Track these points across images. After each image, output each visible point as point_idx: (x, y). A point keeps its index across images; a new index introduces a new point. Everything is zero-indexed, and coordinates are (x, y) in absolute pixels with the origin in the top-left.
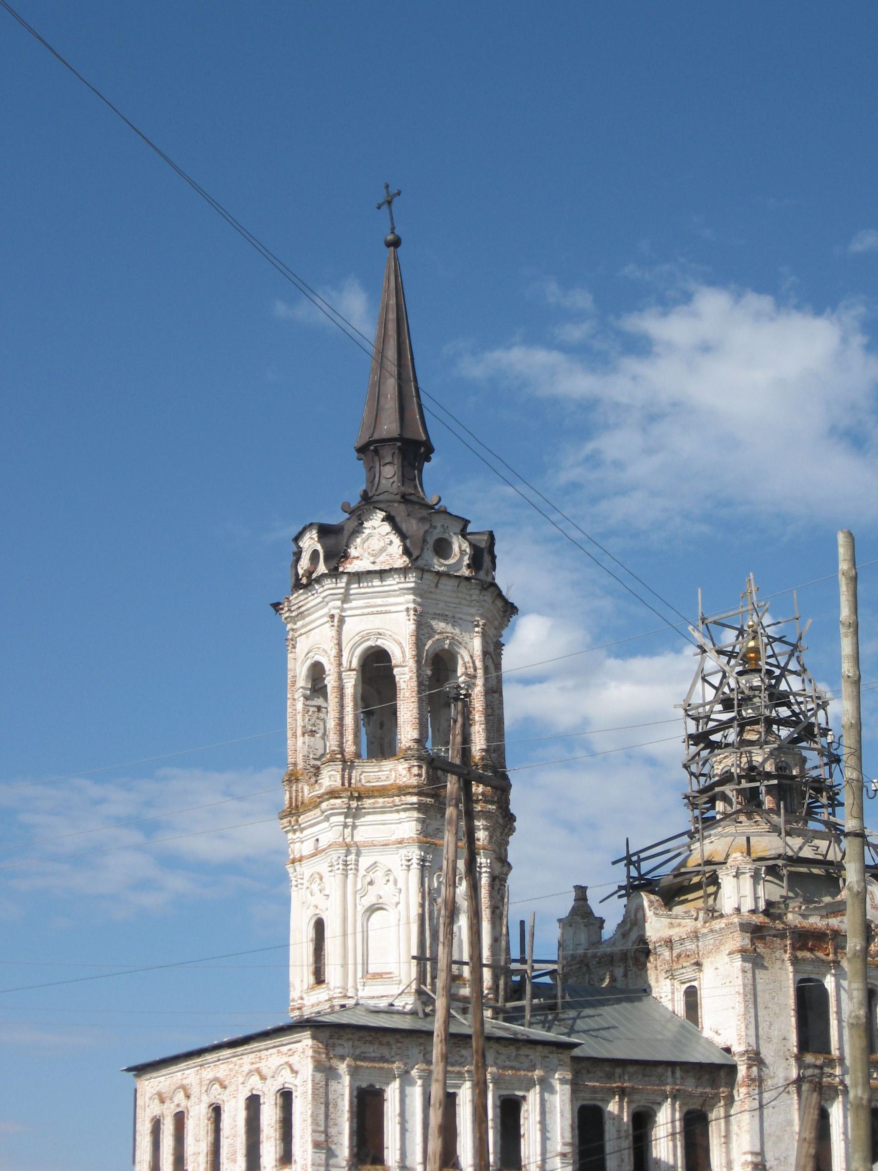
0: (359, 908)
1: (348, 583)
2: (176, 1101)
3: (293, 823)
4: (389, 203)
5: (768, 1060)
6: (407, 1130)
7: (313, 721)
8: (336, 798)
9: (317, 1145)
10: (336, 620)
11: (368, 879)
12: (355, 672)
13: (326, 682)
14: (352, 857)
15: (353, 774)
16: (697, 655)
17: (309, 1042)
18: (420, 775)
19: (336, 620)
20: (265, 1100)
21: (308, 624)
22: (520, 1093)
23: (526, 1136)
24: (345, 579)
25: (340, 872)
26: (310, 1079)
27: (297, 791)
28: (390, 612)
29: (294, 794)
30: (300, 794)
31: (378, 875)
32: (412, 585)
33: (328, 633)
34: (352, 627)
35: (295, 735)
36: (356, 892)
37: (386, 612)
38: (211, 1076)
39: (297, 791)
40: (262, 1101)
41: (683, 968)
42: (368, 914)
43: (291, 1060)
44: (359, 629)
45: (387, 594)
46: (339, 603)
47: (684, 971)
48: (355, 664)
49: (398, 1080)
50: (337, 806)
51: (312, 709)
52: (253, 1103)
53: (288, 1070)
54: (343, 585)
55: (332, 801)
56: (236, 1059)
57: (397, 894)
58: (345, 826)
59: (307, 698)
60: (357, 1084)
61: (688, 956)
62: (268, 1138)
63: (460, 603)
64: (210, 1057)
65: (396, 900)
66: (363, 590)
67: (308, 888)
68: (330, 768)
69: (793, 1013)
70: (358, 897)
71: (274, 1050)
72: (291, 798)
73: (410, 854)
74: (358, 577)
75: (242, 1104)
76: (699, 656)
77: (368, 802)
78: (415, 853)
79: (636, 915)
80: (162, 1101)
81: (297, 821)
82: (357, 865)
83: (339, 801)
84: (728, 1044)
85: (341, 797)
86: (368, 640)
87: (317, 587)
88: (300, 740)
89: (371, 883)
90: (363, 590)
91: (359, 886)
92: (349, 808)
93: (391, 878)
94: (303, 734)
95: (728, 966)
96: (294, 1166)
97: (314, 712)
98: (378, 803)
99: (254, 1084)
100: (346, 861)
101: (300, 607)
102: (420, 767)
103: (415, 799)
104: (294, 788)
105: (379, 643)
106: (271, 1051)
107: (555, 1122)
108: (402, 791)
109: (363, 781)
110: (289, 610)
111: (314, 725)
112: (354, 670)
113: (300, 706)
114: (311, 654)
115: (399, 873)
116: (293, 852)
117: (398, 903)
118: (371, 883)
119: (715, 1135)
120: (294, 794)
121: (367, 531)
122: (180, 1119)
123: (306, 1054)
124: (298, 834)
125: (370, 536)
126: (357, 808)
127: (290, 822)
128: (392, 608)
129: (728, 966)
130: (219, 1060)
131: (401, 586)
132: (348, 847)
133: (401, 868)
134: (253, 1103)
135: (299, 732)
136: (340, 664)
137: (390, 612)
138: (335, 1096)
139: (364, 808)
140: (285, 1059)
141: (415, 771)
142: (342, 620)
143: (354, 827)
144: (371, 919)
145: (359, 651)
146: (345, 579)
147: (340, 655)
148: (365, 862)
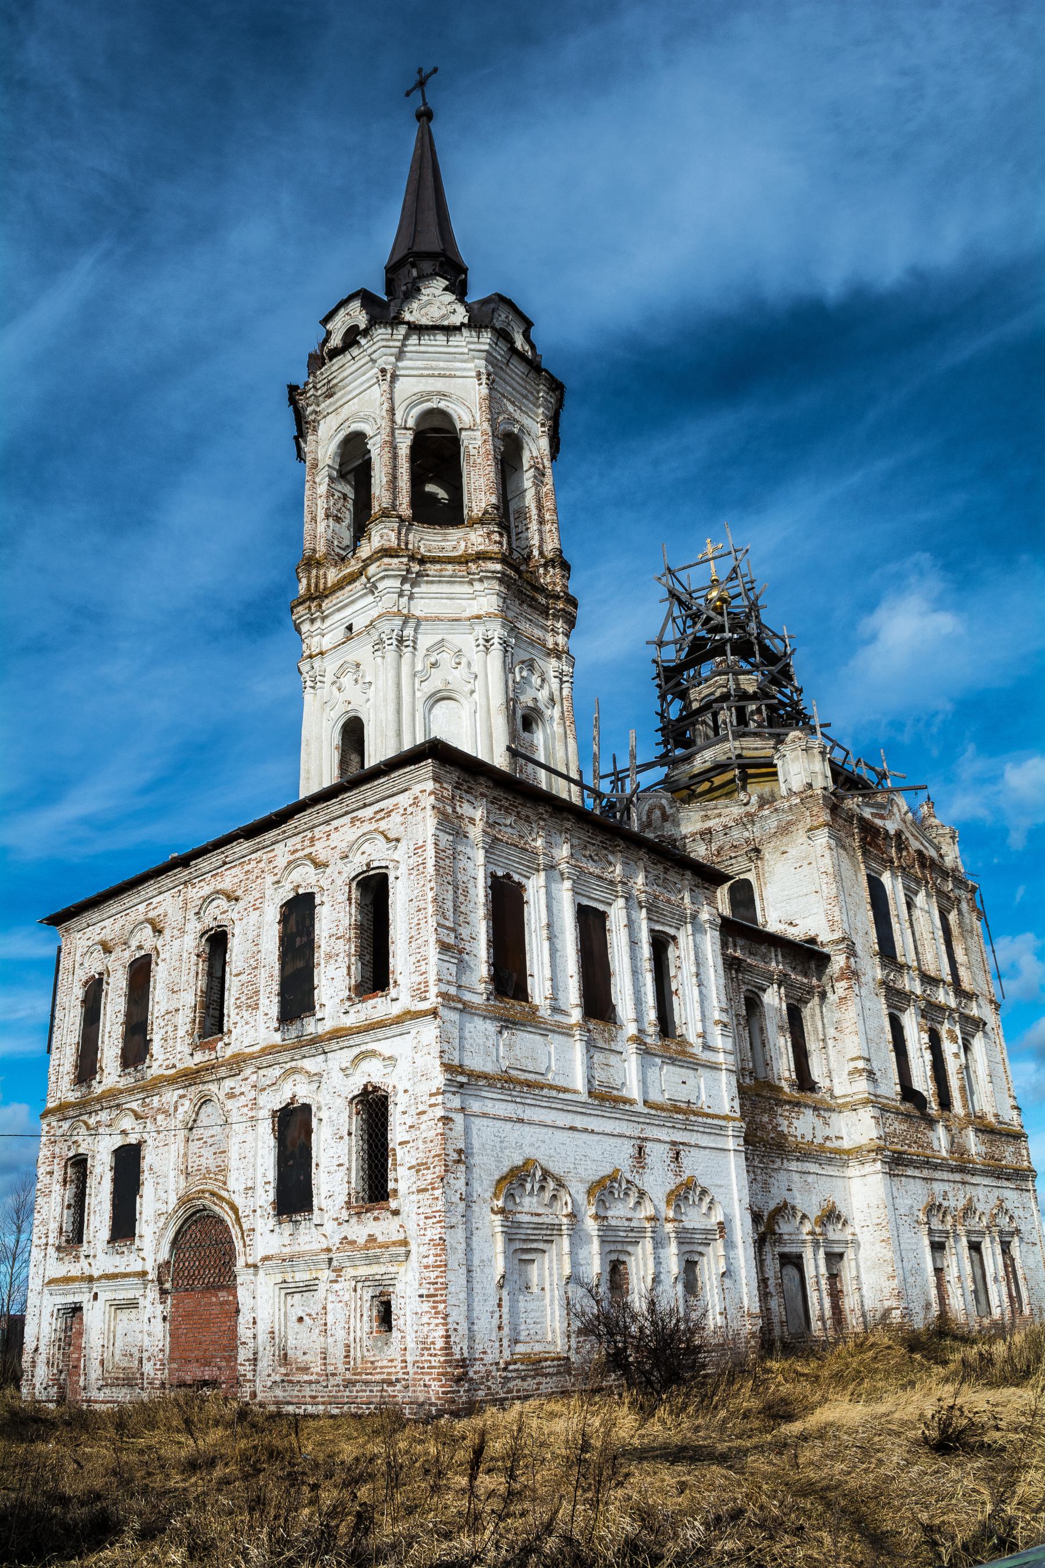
0: (418, 694)
1: (406, 337)
2: (134, 943)
3: (313, 609)
4: (421, 84)
5: (860, 953)
6: (557, 950)
7: (339, 506)
8: (391, 556)
9: (445, 947)
10: (389, 375)
11: (433, 660)
12: (411, 432)
13: (368, 447)
14: (409, 632)
15: (411, 536)
16: (663, 601)
17: (430, 785)
18: (500, 543)
19: (389, 375)
20: (324, 899)
21: (337, 401)
22: (672, 931)
23: (680, 992)
24: (403, 330)
25: (393, 647)
26: (430, 841)
27: (317, 577)
28: (455, 376)
29: (313, 581)
30: (322, 581)
31: (446, 658)
32: (487, 347)
33: (377, 394)
34: (406, 387)
35: (314, 519)
36: (415, 675)
37: (450, 376)
38: (207, 890)
39: (317, 577)
40: (317, 901)
41: (731, 858)
42: (431, 701)
43: (383, 825)
44: (416, 390)
45: (453, 356)
46: (393, 359)
47: (733, 861)
48: (411, 423)
49: (542, 874)
50: (393, 566)
51: (337, 494)
52: (299, 912)
53: (381, 838)
54: (401, 337)
55: (386, 560)
56: (259, 853)
57: (472, 681)
58: (401, 595)
59: (331, 478)
60: (492, 868)
61: (735, 847)
62: (329, 956)
63: (525, 397)
64: (204, 864)
65: (470, 687)
66: (422, 349)
67: (334, 683)
68: (380, 526)
69: (869, 907)
70: (417, 681)
71: (347, 819)
72: (309, 585)
73: (489, 633)
74: (415, 329)
75: (272, 914)
76: (668, 603)
77: (432, 569)
78: (497, 631)
79: (648, 817)
80: (107, 950)
81: (320, 606)
82: (414, 642)
83: (396, 560)
84: (812, 934)
85: (398, 556)
86: (428, 400)
87: (363, 341)
88: (321, 527)
89: (434, 665)
90: (422, 349)
91: (419, 667)
92: (408, 571)
93: (464, 661)
94: (327, 516)
95: (805, 846)
96: (393, 992)
97: (339, 498)
98: (446, 570)
99: (305, 878)
100: (402, 637)
101: (329, 382)
102: (501, 535)
103: (498, 567)
104: (314, 572)
105: (442, 405)
106: (335, 823)
107: (709, 978)
108: (481, 557)
109: (422, 550)
110: (314, 387)
111: (339, 510)
112: (410, 429)
113: (322, 489)
114: (347, 424)
115: (473, 654)
116: (309, 647)
117: (473, 692)
118: (434, 665)
119: (812, 1038)
120: (313, 581)
121: (424, 298)
122: (140, 973)
123: (422, 804)
124: (318, 624)
125: (429, 303)
126: (419, 574)
127: (310, 608)
128: (458, 373)
129: (805, 846)
130: (225, 863)
131: (472, 347)
132: (406, 619)
133: (475, 649)
134: (299, 912)
135: (321, 514)
136: (393, 422)
137: (455, 376)
138: (465, 879)
139: (428, 576)
140: (367, 827)
141: (496, 537)
142: (394, 377)
143: (411, 597)
144: (434, 710)
145: (416, 411)
146: (403, 330)
147: (392, 411)
148: (425, 641)
